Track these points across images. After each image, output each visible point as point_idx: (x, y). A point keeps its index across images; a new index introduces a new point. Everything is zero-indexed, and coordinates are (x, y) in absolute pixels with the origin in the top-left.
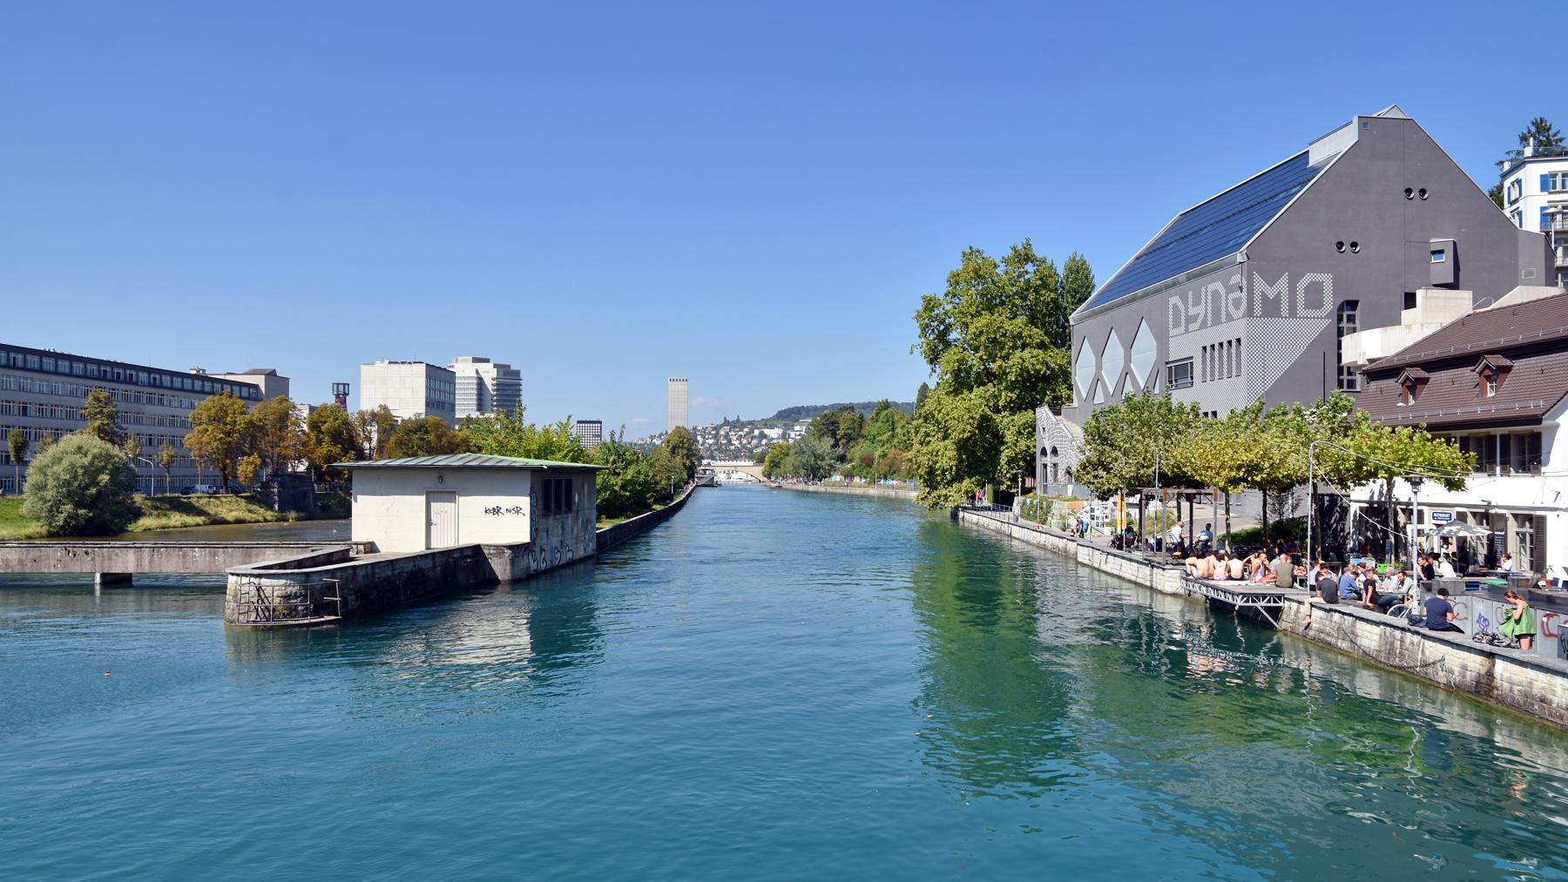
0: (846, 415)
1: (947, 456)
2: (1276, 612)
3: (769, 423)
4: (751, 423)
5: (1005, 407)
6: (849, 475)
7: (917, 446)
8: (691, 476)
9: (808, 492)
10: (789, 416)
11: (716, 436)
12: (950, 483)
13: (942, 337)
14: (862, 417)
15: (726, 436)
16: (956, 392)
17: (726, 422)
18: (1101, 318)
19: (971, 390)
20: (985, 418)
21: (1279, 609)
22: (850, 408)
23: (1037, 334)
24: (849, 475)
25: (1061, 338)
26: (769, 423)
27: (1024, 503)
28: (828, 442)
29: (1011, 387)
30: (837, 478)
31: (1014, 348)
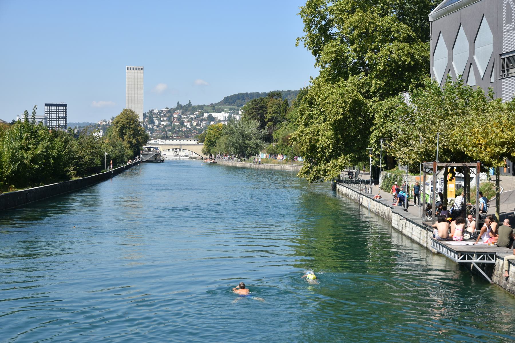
0: (274, 100)
1: (326, 137)
2: (490, 269)
3: (217, 108)
4: (201, 107)
5: (374, 93)
6: (273, 153)
7: (302, 127)
8: (137, 153)
9: (236, 168)
10: (233, 101)
11: (170, 119)
12: (328, 160)
13: (324, 30)
14: (286, 103)
15: (179, 119)
16: (334, 80)
17: (179, 107)
18: (453, 15)
19: (346, 79)
20: (356, 102)
21: (493, 266)
22: (277, 95)
23: (405, 29)
24: (273, 153)
25: (424, 34)
26: (217, 108)
27: (386, 175)
28: (255, 124)
29: (380, 76)
30: (263, 155)
31: (383, 41)
